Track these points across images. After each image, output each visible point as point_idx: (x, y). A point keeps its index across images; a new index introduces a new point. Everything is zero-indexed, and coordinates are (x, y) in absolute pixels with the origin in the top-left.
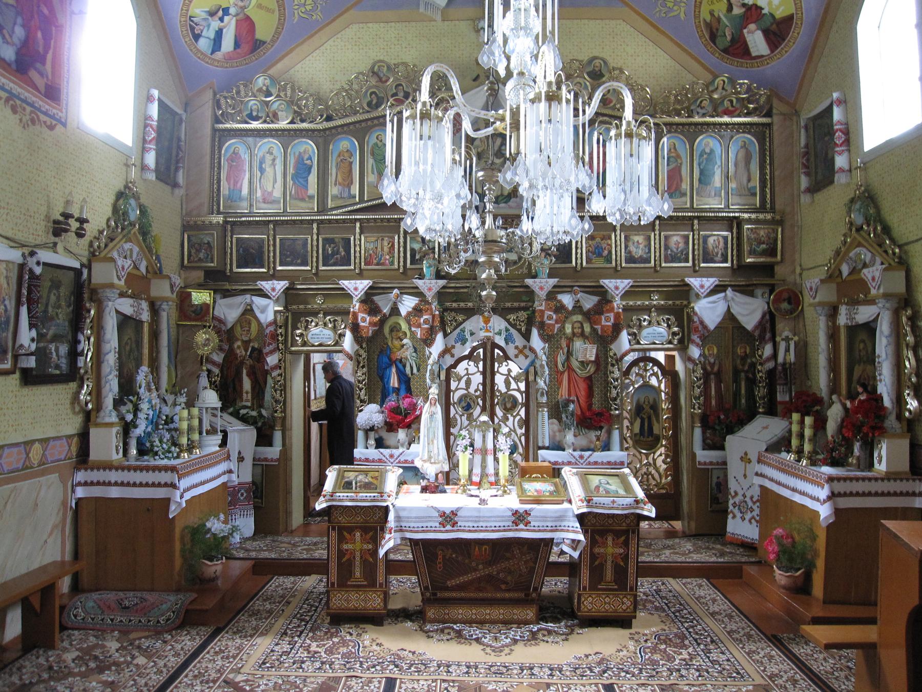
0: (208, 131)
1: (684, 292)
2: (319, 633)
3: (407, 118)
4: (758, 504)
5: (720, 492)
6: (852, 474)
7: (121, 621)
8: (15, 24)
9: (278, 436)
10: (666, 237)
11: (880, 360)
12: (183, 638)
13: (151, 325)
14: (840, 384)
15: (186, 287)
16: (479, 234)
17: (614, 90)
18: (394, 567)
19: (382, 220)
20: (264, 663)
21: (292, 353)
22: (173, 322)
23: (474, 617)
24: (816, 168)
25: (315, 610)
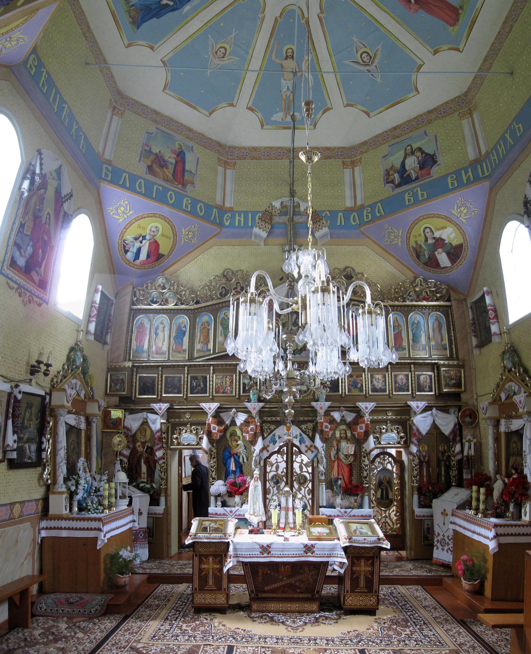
0: (127, 310)
1: (407, 411)
2: (187, 619)
3: (242, 302)
4: (452, 541)
5: (429, 533)
6: (509, 523)
7: (68, 611)
8: (28, 245)
9: (163, 500)
10: (395, 376)
11: (526, 454)
12: (105, 622)
13: (86, 432)
14: (501, 468)
15: (108, 407)
16: (283, 373)
17: (359, 285)
18: (232, 579)
19: (226, 365)
20: (154, 637)
21: (171, 449)
22: (99, 430)
23: (281, 609)
24: (480, 332)
25: (185, 605)
